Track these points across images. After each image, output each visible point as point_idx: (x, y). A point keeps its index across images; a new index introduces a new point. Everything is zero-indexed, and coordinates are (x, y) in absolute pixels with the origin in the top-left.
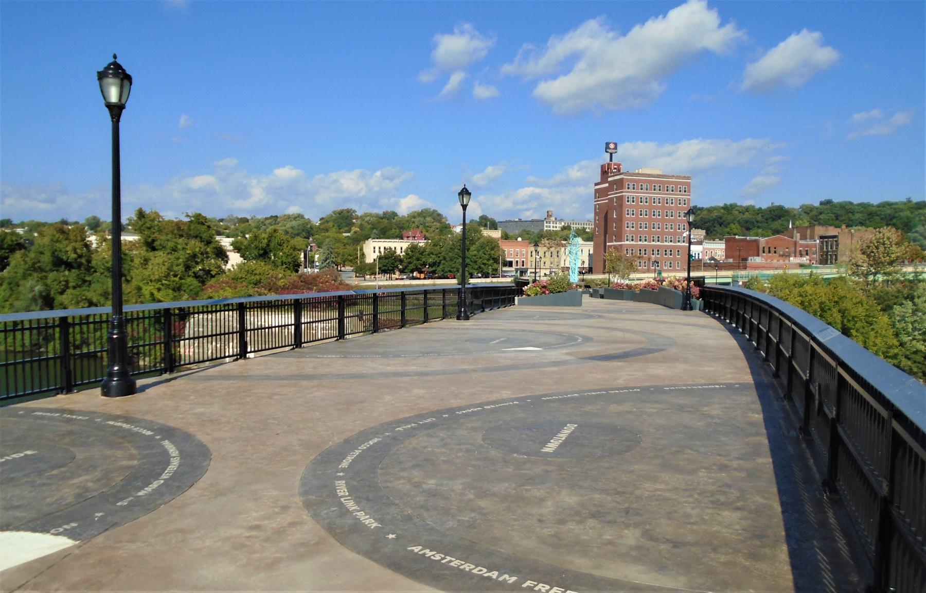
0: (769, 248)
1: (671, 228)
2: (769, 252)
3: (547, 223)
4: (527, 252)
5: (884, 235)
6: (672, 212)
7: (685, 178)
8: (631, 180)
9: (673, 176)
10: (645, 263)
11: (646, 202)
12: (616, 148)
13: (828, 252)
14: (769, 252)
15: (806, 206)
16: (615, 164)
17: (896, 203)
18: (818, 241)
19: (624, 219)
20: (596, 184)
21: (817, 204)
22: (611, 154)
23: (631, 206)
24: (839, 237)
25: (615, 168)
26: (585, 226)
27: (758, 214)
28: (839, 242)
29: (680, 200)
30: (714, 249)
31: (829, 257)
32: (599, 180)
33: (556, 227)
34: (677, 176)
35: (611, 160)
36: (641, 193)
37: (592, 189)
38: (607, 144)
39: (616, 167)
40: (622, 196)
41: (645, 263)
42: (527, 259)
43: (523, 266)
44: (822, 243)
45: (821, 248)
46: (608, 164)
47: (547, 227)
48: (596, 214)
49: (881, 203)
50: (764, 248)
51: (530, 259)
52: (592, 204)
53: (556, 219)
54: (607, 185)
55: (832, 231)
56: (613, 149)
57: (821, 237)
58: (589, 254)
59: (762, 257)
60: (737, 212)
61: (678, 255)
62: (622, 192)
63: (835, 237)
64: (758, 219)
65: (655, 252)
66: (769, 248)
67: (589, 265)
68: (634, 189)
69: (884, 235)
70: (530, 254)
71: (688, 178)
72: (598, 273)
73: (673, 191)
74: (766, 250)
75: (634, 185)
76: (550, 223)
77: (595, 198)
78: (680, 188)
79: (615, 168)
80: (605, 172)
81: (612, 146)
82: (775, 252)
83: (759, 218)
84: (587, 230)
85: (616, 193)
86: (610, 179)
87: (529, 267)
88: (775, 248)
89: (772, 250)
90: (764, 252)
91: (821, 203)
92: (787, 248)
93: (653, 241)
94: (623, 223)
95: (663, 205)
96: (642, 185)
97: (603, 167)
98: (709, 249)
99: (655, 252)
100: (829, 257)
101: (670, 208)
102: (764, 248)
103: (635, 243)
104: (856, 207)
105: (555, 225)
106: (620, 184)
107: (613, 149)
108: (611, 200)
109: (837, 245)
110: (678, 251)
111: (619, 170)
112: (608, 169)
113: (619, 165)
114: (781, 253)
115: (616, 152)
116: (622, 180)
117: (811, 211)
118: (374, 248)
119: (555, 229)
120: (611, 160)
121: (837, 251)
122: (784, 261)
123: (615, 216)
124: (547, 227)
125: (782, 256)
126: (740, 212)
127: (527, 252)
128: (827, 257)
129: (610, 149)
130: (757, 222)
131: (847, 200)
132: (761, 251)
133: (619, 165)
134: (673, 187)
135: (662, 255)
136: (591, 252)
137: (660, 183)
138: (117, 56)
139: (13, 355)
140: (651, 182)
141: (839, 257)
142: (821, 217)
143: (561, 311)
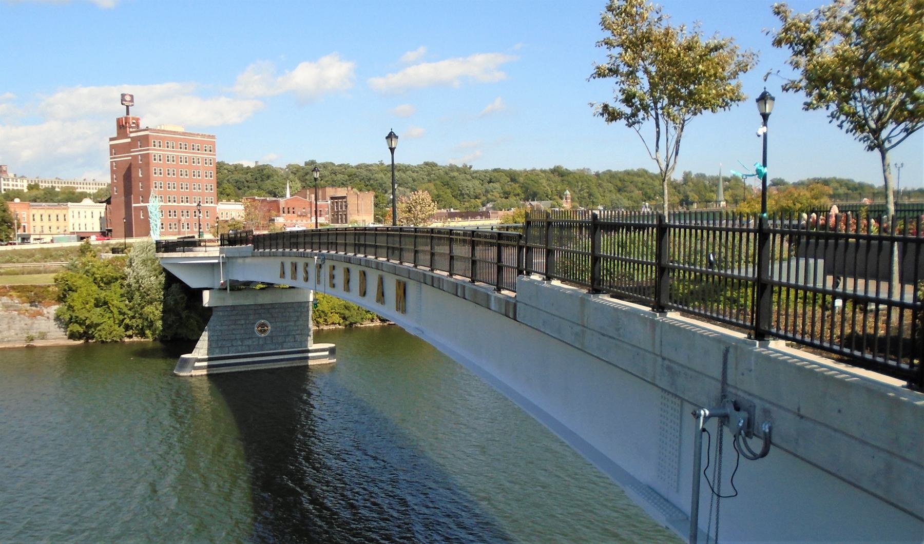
0: (288, 208)
1: (199, 189)
2: (289, 212)
3: (4, 180)
4: (28, 215)
5: (419, 197)
6: (199, 172)
7: (209, 136)
8: (156, 137)
9: (198, 135)
10: (175, 225)
11: (173, 161)
12: (132, 101)
13: (338, 212)
14: (289, 212)
15: (292, 165)
16: (133, 119)
17: (371, 165)
18: (329, 202)
19: (151, 178)
20: (111, 139)
21: (302, 164)
22: (128, 107)
23: (157, 165)
24: (348, 198)
25: (134, 123)
26: (54, 185)
27: (247, 173)
28: (348, 202)
29: (181, 158)
30: (229, 210)
31: (340, 216)
32: (115, 135)
33: (17, 186)
34: (202, 135)
35: (128, 113)
36: (167, 151)
37: (106, 145)
38: (123, 95)
39: (134, 121)
40: (148, 153)
41: (175, 225)
42: (28, 222)
43: (24, 231)
44: (333, 203)
45: (333, 208)
46: (126, 118)
47: (5, 185)
48: (113, 172)
49: (359, 165)
50: (284, 208)
51: (32, 223)
52: (107, 161)
53: (15, 175)
54: (129, 140)
55: (341, 192)
56: (130, 101)
57: (332, 198)
58: (101, 217)
59: (283, 217)
60: (226, 171)
61: (207, 216)
62: (148, 150)
63: (344, 197)
64: (248, 179)
65: (185, 213)
66: (288, 208)
67: (101, 229)
68: (160, 146)
69: (419, 197)
70: (31, 218)
71: (213, 137)
72: (118, 237)
73: (160, 146)
74: (286, 210)
75: (160, 142)
76: (8, 181)
77: (111, 154)
78: (206, 147)
79: (134, 123)
80: (122, 126)
81: (128, 98)
82: (294, 212)
83: (249, 177)
84: (57, 189)
85: (140, 151)
86: (132, 135)
87: (32, 233)
88: (294, 209)
89: (291, 210)
90: (284, 212)
91: (306, 164)
92: (304, 209)
93: (182, 202)
94: (151, 183)
95: (190, 165)
96: (168, 143)
97: (119, 121)
98: (225, 210)
99: (185, 213)
100: (340, 216)
101: (197, 168)
102: (284, 208)
103: (164, 204)
104: (338, 168)
105: (15, 183)
106: (145, 141)
107: (130, 101)
108: (135, 157)
109: (346, 206)
110: (207, 212)
111: (138, 126)
112: (126, 123)
113: (138, 119)
114: (299, 213)
115: (133, 105)
116: (147, 136)
117: (297, 171)
118: (34, 220)
119: (15, 188)
120: (128, 113)
121: (346, 211)
122: (302, 221)
123: (140, 176)
124: (5, 185)
125: (300, 216)
126: (229, 171)
127: (28, 215)
128: (338, 217)
129: (126, 101)
130: (247, 182)
131: (329, 161)
132: (281, 212)
133: (138, 119)
134: (198, 146)
135: (191, 217)
136: (103, 215)
137: (185, 141)
138: (904, 165)
139: (898, 309)
140: (176, 140)
141: (348, 216)
142: (307, 177)
143: (464, 278)
